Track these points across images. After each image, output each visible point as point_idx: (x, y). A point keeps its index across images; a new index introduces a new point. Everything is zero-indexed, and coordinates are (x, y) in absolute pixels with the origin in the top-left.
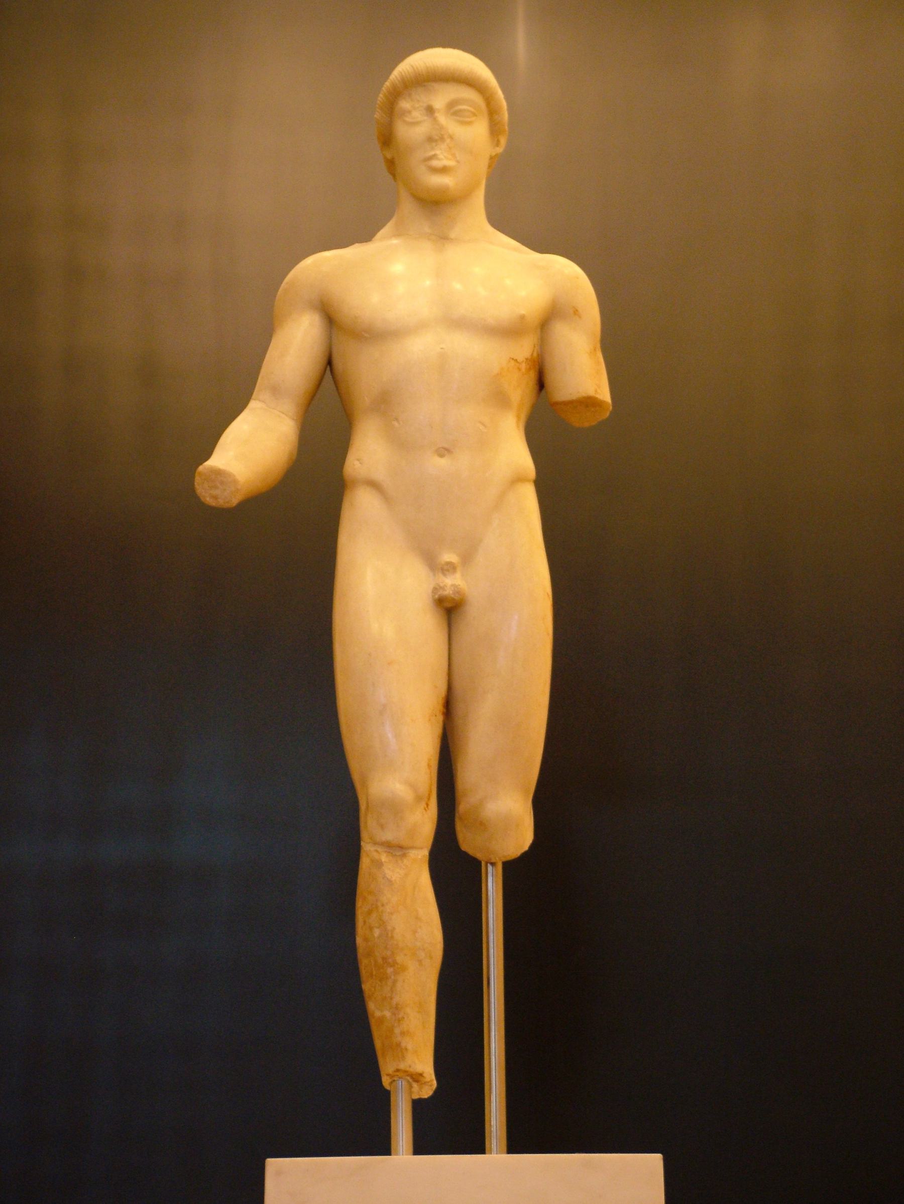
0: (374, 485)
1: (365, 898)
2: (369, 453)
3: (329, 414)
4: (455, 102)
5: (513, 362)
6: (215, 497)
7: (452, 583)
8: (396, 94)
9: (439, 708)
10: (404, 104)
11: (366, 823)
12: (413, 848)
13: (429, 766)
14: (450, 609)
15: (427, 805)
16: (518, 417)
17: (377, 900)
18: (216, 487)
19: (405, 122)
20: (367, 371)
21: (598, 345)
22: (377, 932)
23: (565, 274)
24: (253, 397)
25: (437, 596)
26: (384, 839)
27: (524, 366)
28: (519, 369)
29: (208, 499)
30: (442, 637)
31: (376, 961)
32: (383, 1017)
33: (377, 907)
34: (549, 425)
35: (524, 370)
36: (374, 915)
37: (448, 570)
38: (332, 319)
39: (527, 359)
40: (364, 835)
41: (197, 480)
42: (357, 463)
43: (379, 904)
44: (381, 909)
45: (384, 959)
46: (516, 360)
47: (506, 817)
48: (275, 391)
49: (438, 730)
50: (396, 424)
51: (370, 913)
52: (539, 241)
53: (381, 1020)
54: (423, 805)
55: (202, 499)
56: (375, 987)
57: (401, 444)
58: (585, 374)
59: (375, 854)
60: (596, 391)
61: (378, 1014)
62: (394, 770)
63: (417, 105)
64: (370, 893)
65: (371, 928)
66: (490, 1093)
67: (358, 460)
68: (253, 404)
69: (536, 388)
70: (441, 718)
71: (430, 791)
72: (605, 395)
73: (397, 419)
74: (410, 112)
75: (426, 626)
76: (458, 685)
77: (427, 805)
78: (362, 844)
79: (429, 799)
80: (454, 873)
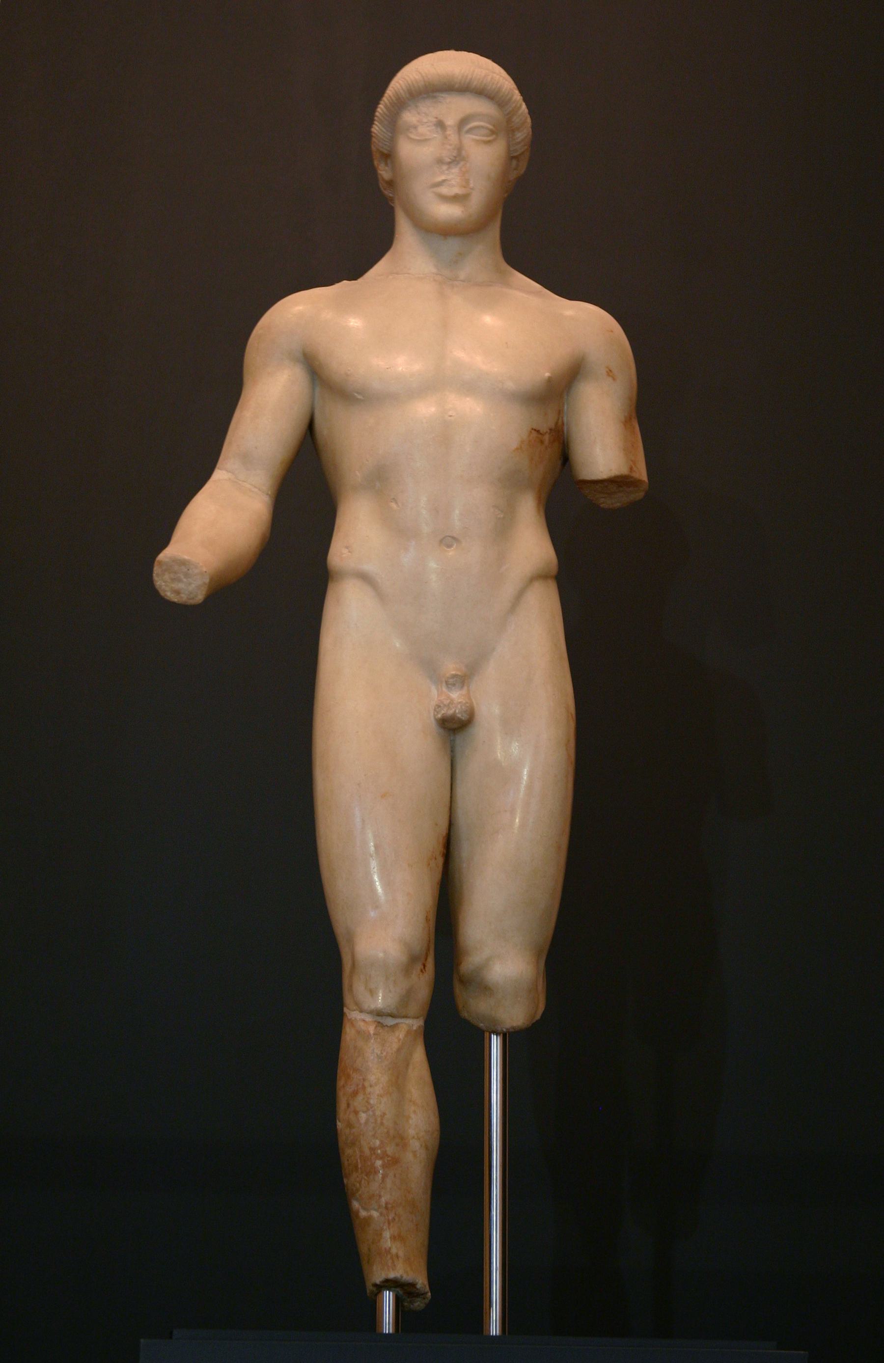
0: (365, 578)
1: (349, 1077)
2: (358, 538)
3: (308, 493)
4: (449, 120)
5: (534, 434)
6: (178, 592)
7: (456, 700)
8: (400, 104)
9: (440, 849)
10: (409, 117)
11: (351, 986)
12: (406, 1017)
13: (427, 920)
14: (454, 728)
15: (424, 966)
16: (539, 499)
17: (364, 1080)
18: (180, 580)
19: (409, 138)
20: (357, 442)
21: (634, 415)
22: (363, 1116)
23: (587, 327)
24: (218, 466)
25: (439, 716)
26: (373, 1007)
27: (547, 438)
28: (542, 442)
29: (169, 594)
30: (439, 734)
31: (362, 1152)
32: (370, 1217)
33: (364, 1088)
34: (564, 497)
35: (547, 442)
36: (360, 1097)
37: (454, 685)
38: (315, 370)
39: (551, 430)
40: (348, 999)
41: (156, 570)
42: (345, 551)
43: (367, 1084)
44: (369, 1090)
45: (373, 1150)
46: (538, 431)
47: (506, 963)
48: (246, 459)
49: (438, 876)
50: (393, 505)
51: (355, 1094)
52: (566, 286)
53: (368, 1221)
54: (419, 966)
55: (162, 594)
56: (360, 1182)
57: (401, 531)
58: (605, 448)
59: (362, 1024)
60: (631, 469)
61: (363, 1214)
62: (377, 905)
63: (425, 120)
64: (356, 1070)
65: (356, 1113)
66: (490, 1306)
67: (347, 547)
68: (219, 475)
69: (560, 463)
70: (440, 861)
71: (428, 949)
72: (642, 473)
73: (395, 500)
74: (415, 127)
75: (418, 744)
76: (462, 820)
77: (424, 966)
78: (345, 1010)
79: (426, 959)
80: (449, 1036)
